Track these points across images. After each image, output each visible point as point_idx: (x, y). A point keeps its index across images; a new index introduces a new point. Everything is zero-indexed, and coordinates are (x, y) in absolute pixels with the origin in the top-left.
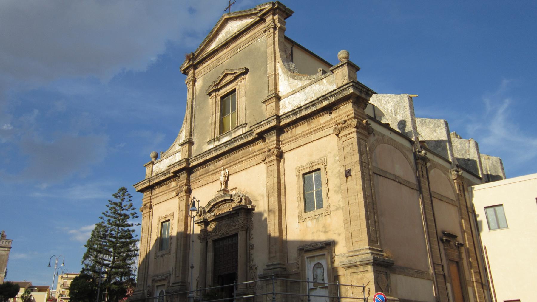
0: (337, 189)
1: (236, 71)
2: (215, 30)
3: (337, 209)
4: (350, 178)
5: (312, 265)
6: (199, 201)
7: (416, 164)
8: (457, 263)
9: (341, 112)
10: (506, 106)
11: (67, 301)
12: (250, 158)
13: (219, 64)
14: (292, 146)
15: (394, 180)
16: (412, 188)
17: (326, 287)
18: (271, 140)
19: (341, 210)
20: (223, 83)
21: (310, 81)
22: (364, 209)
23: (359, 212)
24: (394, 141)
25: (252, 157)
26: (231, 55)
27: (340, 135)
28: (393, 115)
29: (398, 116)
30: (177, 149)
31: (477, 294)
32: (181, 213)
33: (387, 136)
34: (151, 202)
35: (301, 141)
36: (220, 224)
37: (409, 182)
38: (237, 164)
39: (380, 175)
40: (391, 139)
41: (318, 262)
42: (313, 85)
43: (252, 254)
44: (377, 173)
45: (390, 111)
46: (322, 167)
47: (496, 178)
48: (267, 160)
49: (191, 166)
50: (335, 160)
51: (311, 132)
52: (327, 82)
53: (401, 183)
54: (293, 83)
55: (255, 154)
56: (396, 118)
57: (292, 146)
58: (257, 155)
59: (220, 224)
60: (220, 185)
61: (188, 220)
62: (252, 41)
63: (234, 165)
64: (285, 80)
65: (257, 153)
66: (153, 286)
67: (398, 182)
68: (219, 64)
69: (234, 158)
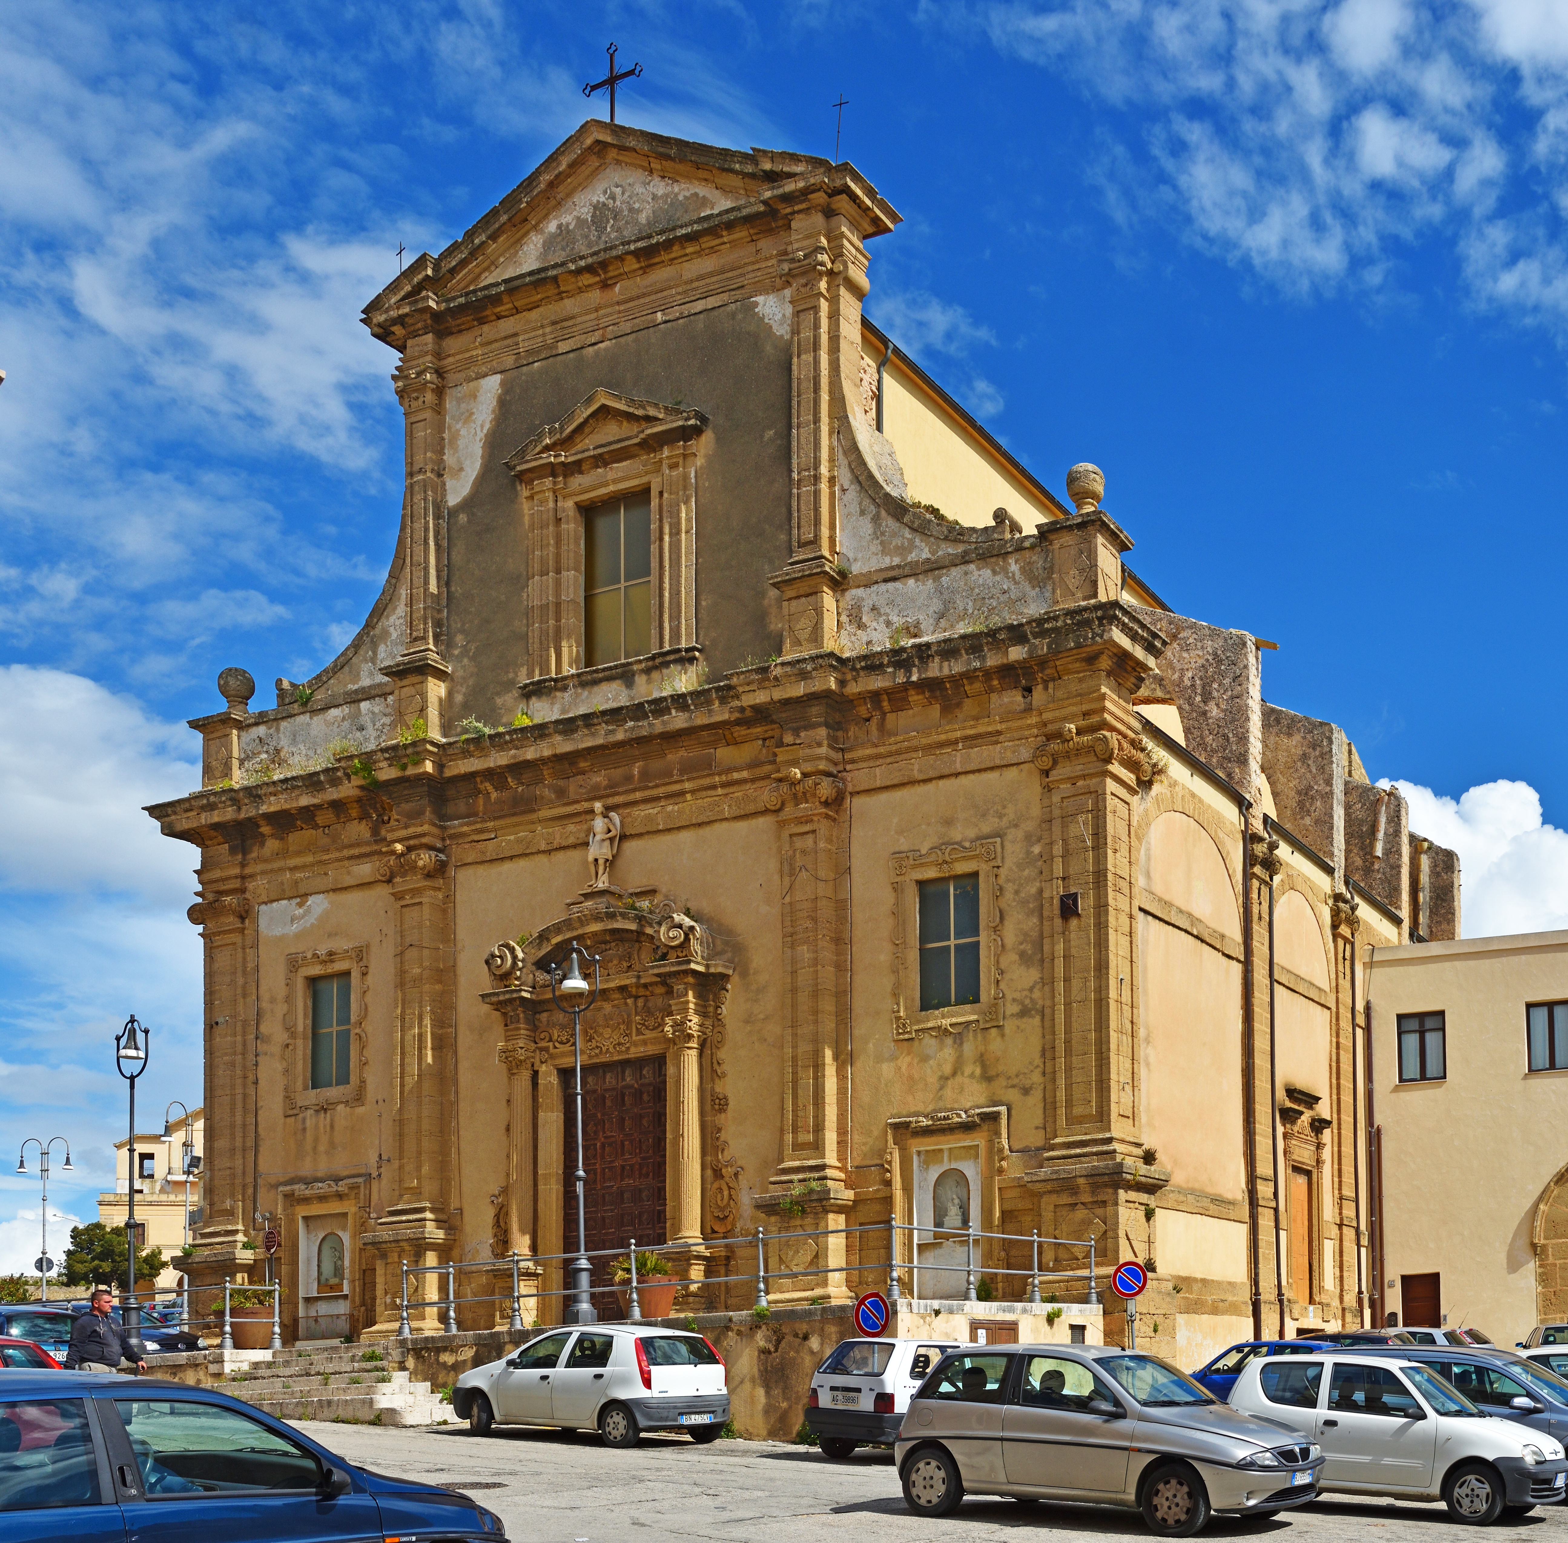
0: (1028, 948)
1: (652, 412)
2: (546, 178)
3: (1024, 1013)
4: (1074, 923)
5: (934, 1174)
6: (146, 1032)
7: (1248, 876)
8: (1308, 1173)
9: (681, 1457)
10: (994, 342)
11: (1487, 833)
12: (714, 787)
13: (563, 347)
14: (880, 775)
15: (1186, 931)
16: (1229, 957)
17: (345, 1297)
18: (815, 746)
19: (1037, 1020)
20: (589, 444)
21: (960, 548)
22: (1320, 1516)
23: (620, 897)
24: (1201, 801)
25: (724, 785)
26: (627, 327)
27: (1054, 775)
28: (1198, 698)
29: (1212, 705)
30: (366, 682)
31: (667, 594)
32: (1126, 1077)
33: (1184, 787)
34: (243, 891)
35: (917, 766)
36: (313, 1313)
37: (1223, 936)
38: (657, 799)
39: (1155, 917)
40: (1193, 795)
41: (954, 1165)
42: (972, 567)
43: (1316, 292)
44: (1147, 908)
45: (1188, 683)
46: (984, 868)
47: (1425, 941)
48: (789, 811)
49: (448, 773)
50: (1028, 853)
51: (956, 742)
52: (1023, 570)
53: (1202, 941)
54: (894, 535)
55: (736, 776)
56: (1205, 713)
57: (880, 775)
58: (744, 781)
59: (1049, 1257)
60: (1302, 1082)
61: (831, 363)
62: (725, 297)
63: (646, 801)
64: (862, 513)
65: (745, 774)
66: (292, 1221)
67: (1197, 937)
68: (563, 347)
69: (645, 775)
